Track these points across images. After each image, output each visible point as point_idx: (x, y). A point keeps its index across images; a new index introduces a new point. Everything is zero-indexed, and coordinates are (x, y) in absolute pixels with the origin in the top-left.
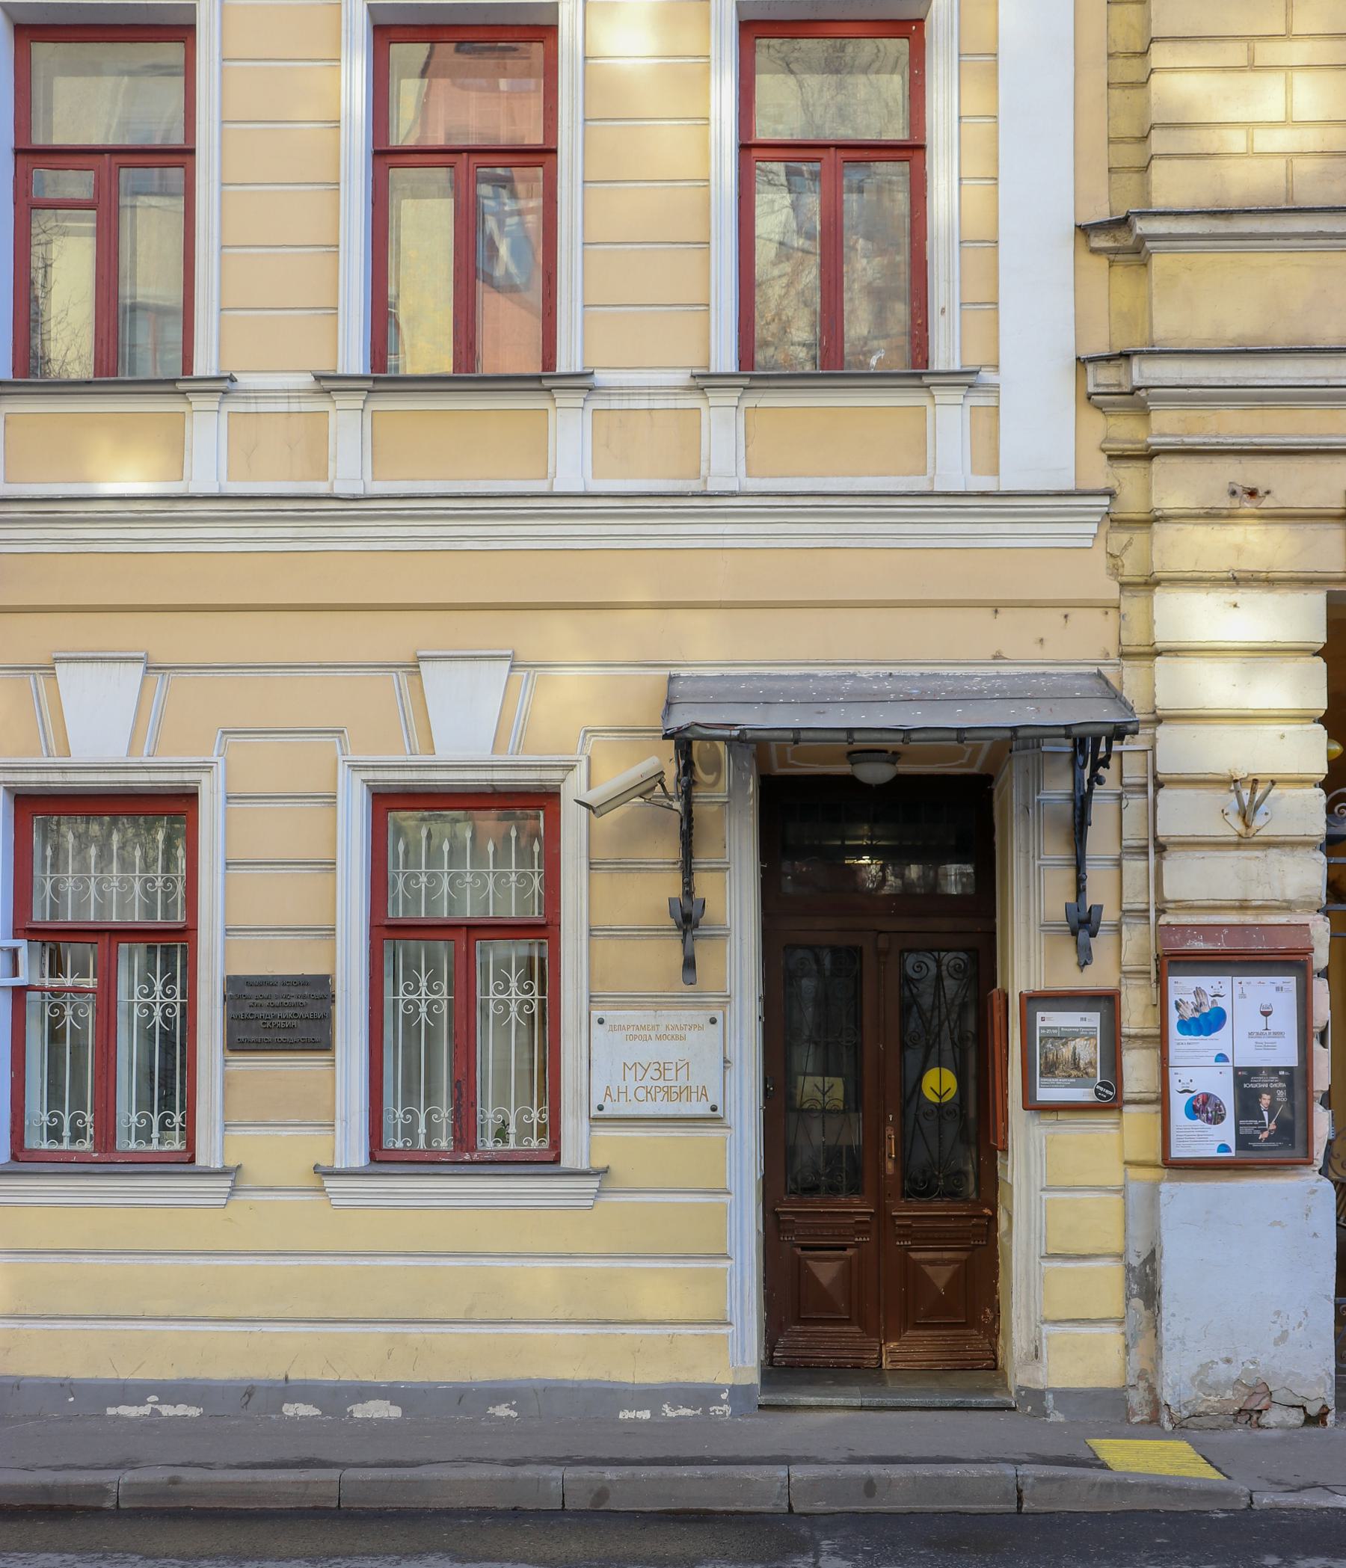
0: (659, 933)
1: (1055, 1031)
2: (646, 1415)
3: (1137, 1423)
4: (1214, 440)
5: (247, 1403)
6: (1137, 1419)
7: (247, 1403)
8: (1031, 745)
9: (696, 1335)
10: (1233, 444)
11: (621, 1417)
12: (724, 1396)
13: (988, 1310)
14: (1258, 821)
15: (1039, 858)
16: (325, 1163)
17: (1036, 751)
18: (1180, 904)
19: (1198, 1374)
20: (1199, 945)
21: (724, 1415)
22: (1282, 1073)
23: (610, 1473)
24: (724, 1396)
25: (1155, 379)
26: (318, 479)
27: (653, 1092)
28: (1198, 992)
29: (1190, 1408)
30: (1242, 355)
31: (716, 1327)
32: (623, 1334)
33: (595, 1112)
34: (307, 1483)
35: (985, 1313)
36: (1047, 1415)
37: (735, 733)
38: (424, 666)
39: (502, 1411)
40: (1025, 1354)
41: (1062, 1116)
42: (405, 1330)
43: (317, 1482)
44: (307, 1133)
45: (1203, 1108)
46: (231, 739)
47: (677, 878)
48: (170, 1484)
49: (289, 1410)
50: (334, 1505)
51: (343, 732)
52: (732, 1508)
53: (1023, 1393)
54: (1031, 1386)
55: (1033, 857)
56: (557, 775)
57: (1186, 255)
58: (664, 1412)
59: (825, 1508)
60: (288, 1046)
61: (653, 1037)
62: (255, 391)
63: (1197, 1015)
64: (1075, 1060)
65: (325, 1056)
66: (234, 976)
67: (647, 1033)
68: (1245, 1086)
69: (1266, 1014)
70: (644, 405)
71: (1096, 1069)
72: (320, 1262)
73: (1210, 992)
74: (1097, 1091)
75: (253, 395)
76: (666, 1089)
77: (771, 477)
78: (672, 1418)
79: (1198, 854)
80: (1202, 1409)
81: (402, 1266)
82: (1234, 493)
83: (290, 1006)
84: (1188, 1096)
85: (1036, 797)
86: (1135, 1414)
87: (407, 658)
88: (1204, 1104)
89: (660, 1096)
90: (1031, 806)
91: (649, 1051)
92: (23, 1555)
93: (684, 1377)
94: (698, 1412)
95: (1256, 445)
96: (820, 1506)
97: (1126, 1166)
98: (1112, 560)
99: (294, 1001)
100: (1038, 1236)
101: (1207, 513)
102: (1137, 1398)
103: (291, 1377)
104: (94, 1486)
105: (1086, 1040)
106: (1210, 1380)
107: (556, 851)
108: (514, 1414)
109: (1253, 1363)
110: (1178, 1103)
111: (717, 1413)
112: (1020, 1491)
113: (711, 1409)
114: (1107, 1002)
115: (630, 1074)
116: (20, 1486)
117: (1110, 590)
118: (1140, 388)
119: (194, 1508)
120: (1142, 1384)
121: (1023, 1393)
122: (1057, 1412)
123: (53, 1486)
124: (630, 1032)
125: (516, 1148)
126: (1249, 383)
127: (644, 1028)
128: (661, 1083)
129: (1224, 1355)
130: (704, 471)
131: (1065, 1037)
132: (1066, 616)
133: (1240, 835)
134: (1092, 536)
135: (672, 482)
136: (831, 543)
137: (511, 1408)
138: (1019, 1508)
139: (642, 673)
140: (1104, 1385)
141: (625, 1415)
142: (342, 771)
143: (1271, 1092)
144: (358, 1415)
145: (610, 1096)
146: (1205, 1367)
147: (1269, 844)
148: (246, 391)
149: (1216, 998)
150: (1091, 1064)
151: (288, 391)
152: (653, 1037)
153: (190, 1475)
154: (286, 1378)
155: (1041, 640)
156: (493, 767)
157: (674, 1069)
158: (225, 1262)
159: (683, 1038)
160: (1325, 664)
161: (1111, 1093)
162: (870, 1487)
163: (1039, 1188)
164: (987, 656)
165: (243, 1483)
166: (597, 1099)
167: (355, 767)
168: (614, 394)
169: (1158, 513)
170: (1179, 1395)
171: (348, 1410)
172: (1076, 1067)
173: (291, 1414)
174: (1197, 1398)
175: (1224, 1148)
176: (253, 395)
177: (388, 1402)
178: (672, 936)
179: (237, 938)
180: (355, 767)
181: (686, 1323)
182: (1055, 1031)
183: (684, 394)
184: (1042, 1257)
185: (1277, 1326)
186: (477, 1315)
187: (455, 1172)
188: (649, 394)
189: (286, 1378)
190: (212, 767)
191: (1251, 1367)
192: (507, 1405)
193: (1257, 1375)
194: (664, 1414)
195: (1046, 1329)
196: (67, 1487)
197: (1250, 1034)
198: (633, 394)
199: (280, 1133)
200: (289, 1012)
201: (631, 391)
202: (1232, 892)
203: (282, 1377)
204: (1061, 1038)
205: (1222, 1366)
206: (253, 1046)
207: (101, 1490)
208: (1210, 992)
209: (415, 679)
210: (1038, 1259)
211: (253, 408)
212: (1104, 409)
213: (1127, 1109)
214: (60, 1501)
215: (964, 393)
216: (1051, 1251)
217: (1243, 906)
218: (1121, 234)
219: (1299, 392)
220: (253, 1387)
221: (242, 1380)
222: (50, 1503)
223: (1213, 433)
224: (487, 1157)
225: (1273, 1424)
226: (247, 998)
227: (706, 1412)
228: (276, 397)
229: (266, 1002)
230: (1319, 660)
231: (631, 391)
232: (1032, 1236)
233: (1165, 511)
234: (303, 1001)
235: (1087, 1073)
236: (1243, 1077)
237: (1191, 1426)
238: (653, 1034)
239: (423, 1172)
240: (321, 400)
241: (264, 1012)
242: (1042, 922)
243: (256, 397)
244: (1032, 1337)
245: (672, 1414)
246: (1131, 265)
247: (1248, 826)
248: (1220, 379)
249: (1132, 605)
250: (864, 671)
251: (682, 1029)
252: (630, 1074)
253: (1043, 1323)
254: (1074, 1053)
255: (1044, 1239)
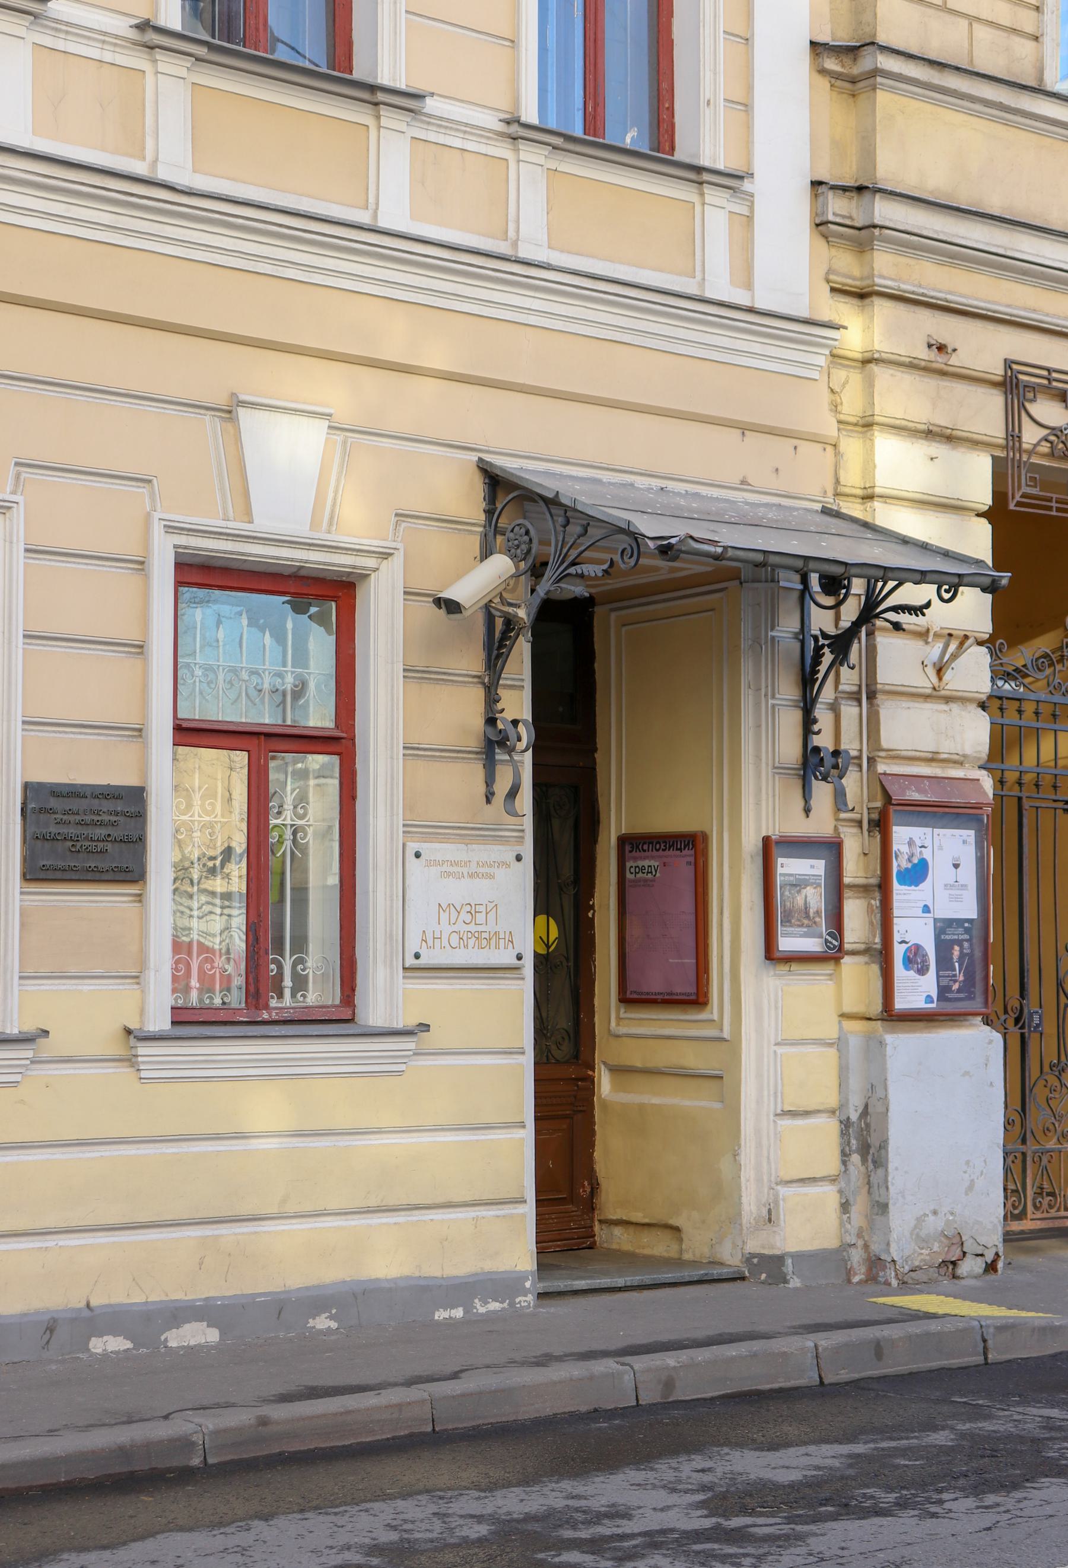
0: (443, 754)
1: (792, 878)
2: (458, 1313)
3: (857, 1283)
4: (921, 291)
5: (48, 1342)
6: (856, 1279)
7: (48, 1342)
8: (763, 579)
9: (498, 1216)
10: (932, 297)
11: (436, 1318)
12: (528, 1284)
13: (586, 1183)
14: (948, 676)
15: (773, 697)
16: (133, 1025)
17: (772, 585)
18: (890, 753)
19: (915, 1227)
20: (916, 796)
21: (529, 1306)
22: (966, 925)
23: (671, 1360)
24: (528, 1284)
25: (891, 220)
26: (131, 156)
27: (465, 938)
28: (911, 843)
29: (910, 1263)
30: (943, 210)
31: (511, 1206)
32: (432, 1220)
33: (410, 961)
34: (399, 1406)
35: (583, 1186)
36: (786, 1281)
37: (719, 550)
38: (242, 413)
39: (322, 1323)
40: (755, 1219)
41: (794, 967)
42: (216, 1232)
43: (409, 1403)
44: (111, 987)
45: (915, 959)
46: (26, 473)
47: (479, 693)
48: (259, 1425)
49: (98, 1345)
50: (429, 1429)
51: (150, 481)
52: (776, 1386)
53: (755, 1261)
54: (766, 1252)
55: (766, 695)
56: (370, 562)
57: (901, 97)
58: (476, 1308)
59: (848, 1376)
60: (97, 876)
61: (466, 874)
62: (68, 24)
63: (909, 866)
64: (806, 908)
65: (133, 889)
66: (38, 783)
67: (459, 869)
68: (943, 937)
69: (956, 866)
70: (457, 143)
71: (821, 918)
72: (438, 1139)
73: (919, 843)
74: (826, 941)
75: (64, 28)
76: (476, 935)
77: (569, 252)
78: (482, 1315)
79: (905, 704)
80: (917, 1263)
81: (213, 1151)
82: (930, 346)
83: (101, 824)
84: (904, 946)
85: (770, 633)
86: (855, 1274)
87: (221, 399)
88: (915, 954)
89: (471, 942)
90: (763, 642)
91: (458, 891)
92: (341, 1509)
93: (489, 1266)
94: (505, 1305)
95: (947, 301)
96: (844, 1376)
97: (841, 1019)
98: (832, 396)
99: (106, 818)
100: (772, 1092)
101: (910, 362)
102: (856, 1257)
103: (94, 1303)
104: (178, 1439)
105: (815, 888)
106: (923, 1234)
107: (351, 652)
108: (334, 1325)
109: (952, 1214)
110: (899, 952)
111: (523, 1304)
112: (985, 1341)
113: (517, 1300)
114: (832, 849)
115: (444, 917)
116: (93, 1452)
117: (830, 429)
118: (875, 226)
119: (289, 1452)
120: (860, 1243)
121: (755, 1261)
122: (794, 1277)
123: (132, 1446)
124: (445, 868)
125: (293, 1005)
126: (1009, 253)
127: (457, 864)
128: (472, 928)
129: (932, 1208)
130: (511, 233)
131: (799, 884)
132: (795, 448)
133: (934, 688)
134: (819, 369)
135: (490, 241)
136: (618, 337)
137: (331, 1318)
138: (986, 1358)
139: (448, 455)
140: (825, 1246)
141: (441, 1315)
142: (157, 529)
143: (960, 943)
144: (173, 1344)
145: (426, 942)
146: (920, 1220)
147: (948, 699)
148: (430, 116)
149: (923, 849)
150: (818, 913)
151: (105, 34)
152: (466, 874)
153: (280, 1412)
154: (88, 1305)
155: (777, 470)
156: (310, 546)
157: (484, 913)
158: (15, 1158)
159: (491, 877)
160: (990, 527)
161: (836, 943)
162: (878, 1349)
163: (773, 1042)
164: (735, 480)
165: (336, 1414)
166: (413, 944)
167: (171, 529)
168: (433, 124)
169: (876, 356)
170: (902, 1250)
171: (163, 1338)
172: (808, 917)
173: (99, 1351)
174: (915, 1251)
175: (929, 999)
176: (64, 28)
177: (205, 1324)
178: (789, 774)
179: (32, 733)
180: (171, 529)
181: (486, 1204)
182: (792, 878)
183: (496, 140)
184: (776, 1115)
185: (967, 1175)
186: (291, 1208)
187: (283, 1033)
188: (465, 132)
189: (88, 1305)
190: (9, 508)
191: (951, 1218)
192: (327, 1314)
193: (955, 1226)
194: (475, 1311)
195: (782, 1191)
196: (148, 1446)
197: (945, 885)
198: (451, 128)
199: (80, 987)
200: (102, 832)
201: (451, 125)
202: (926, 744)
203: (83, 1304)
204: (795, 885)
205: (931, 1218)
206: (59, 875)
207: (185, 1444)
208: (919, 843)
209: (229, 426)
210: (772, 1117)
211: (60, 45)
212: (830, 239)
213: (847, 960)
214: (140, 1466)
215: (546, 154)
216: (787, 1108)
217: (933, 759)
218: (847, 60)
219: (988, 258)
220: (55, 1320)
221: (37, 1313)
222: (130, 1469)
223: (916, 282)
224: (286, 1015)
225: (965, 1274)
226: (51, 811)
227: (512, 1304)
228: (89, 38)
229: (72, 818)
230: (984, 521)
231: (451, 125)
232: (766, 1093)
233: (883, 354)
234: (113, 818)
235: (815, 923)
236: (943, 927)
237: (910, 1281)
238: (465, 870)
239: (250, 1034)
240: (138, 54)
241: (72, 831)
242: (777, 764)
243: (67, 32)
244: (764, 1200)
245: (482, 1310)
246: (843, 93)
247: (940, 679)
248: (936, 232)
249: (852, 446)
250: (641, 482)
251: (491, 866)
252: (444, 917)
253: (777, 1184)
254: (806, 901)
255: (779, 1095)
